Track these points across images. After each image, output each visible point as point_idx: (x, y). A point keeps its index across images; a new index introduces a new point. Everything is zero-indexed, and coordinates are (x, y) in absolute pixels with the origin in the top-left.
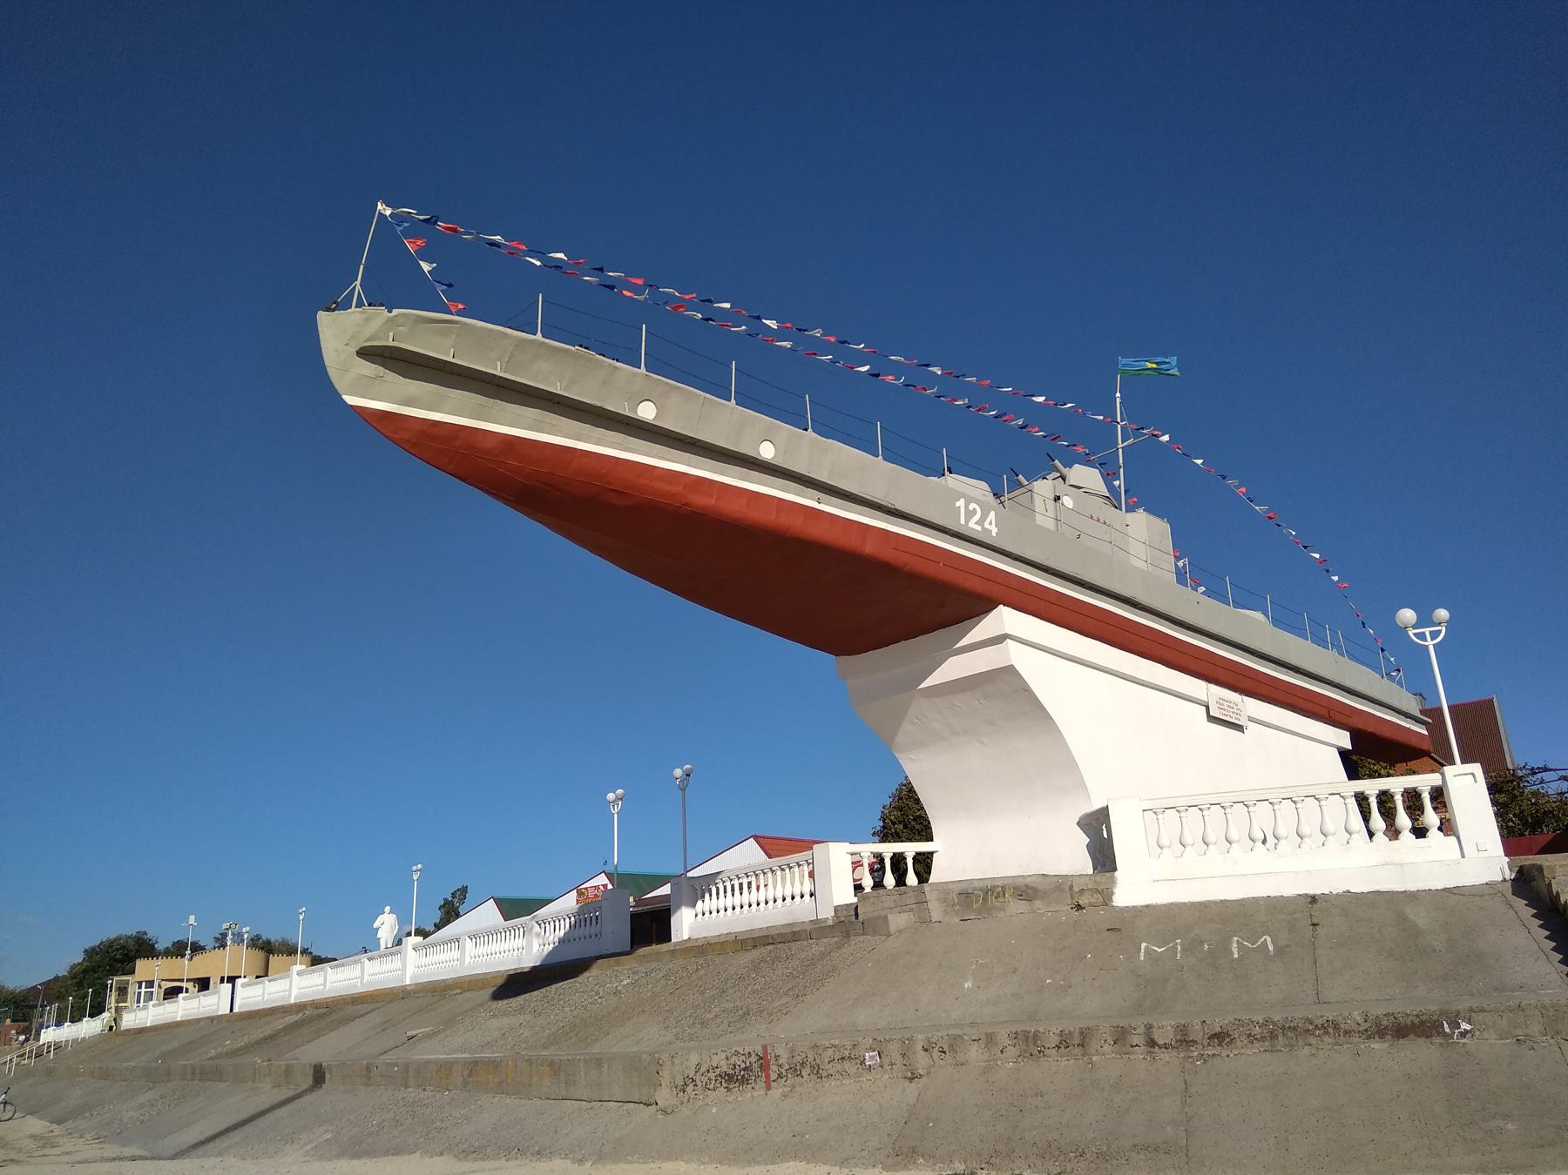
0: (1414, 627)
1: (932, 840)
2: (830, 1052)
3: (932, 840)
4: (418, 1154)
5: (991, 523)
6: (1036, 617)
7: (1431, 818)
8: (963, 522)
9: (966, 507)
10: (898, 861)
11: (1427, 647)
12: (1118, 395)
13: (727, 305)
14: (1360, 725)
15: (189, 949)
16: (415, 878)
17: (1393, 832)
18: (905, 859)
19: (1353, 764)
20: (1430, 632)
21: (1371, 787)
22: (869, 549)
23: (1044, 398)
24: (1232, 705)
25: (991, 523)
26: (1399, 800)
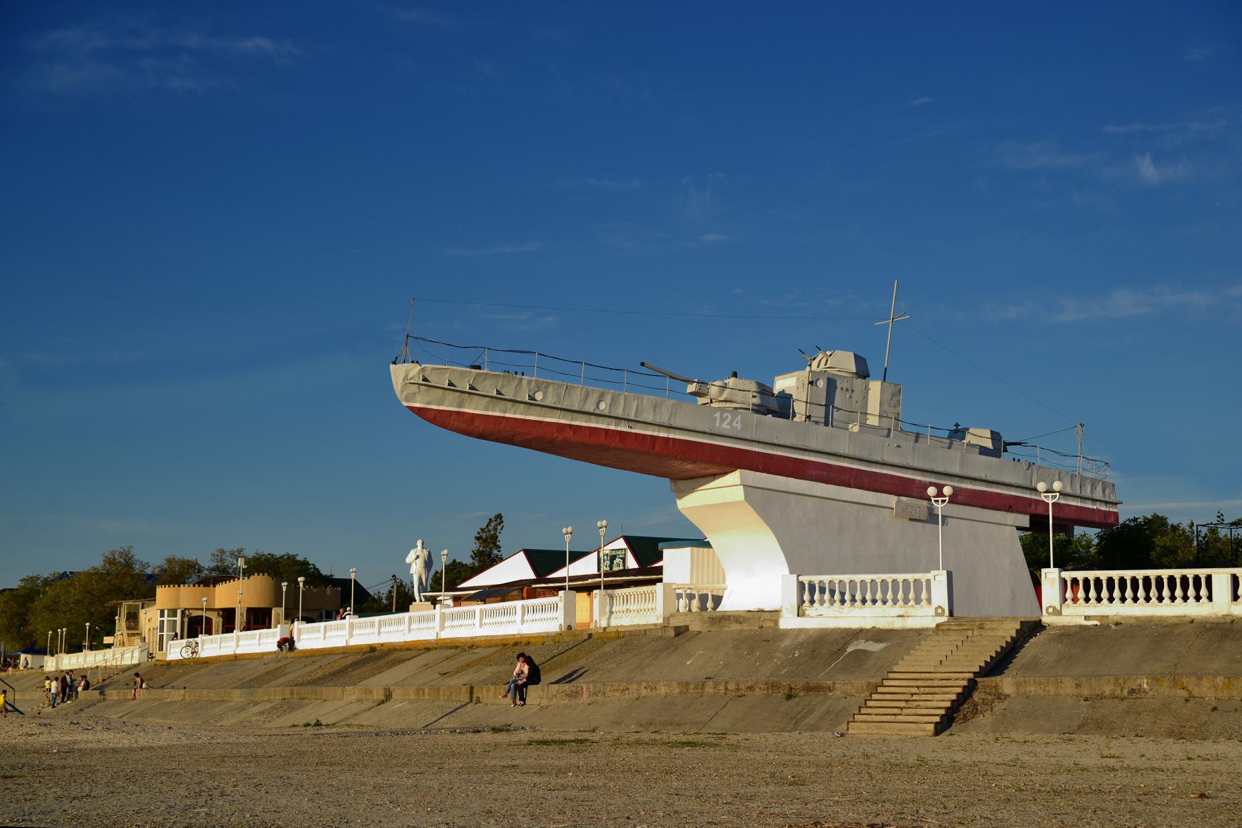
0: (934, 497)
1: (234, 609)
2: (609, 687)
3: (234, 609)
5: (737, 423)
7: (1204, 592)
8: (717, 425)
9: (721, 416)
11: (938, 507)
15: (88, 628)
16: (602, 534)
17: (832, 602)
18: (1188, 579)
20: (176, 620)
25: (737, 423)
26: (1117, 583)
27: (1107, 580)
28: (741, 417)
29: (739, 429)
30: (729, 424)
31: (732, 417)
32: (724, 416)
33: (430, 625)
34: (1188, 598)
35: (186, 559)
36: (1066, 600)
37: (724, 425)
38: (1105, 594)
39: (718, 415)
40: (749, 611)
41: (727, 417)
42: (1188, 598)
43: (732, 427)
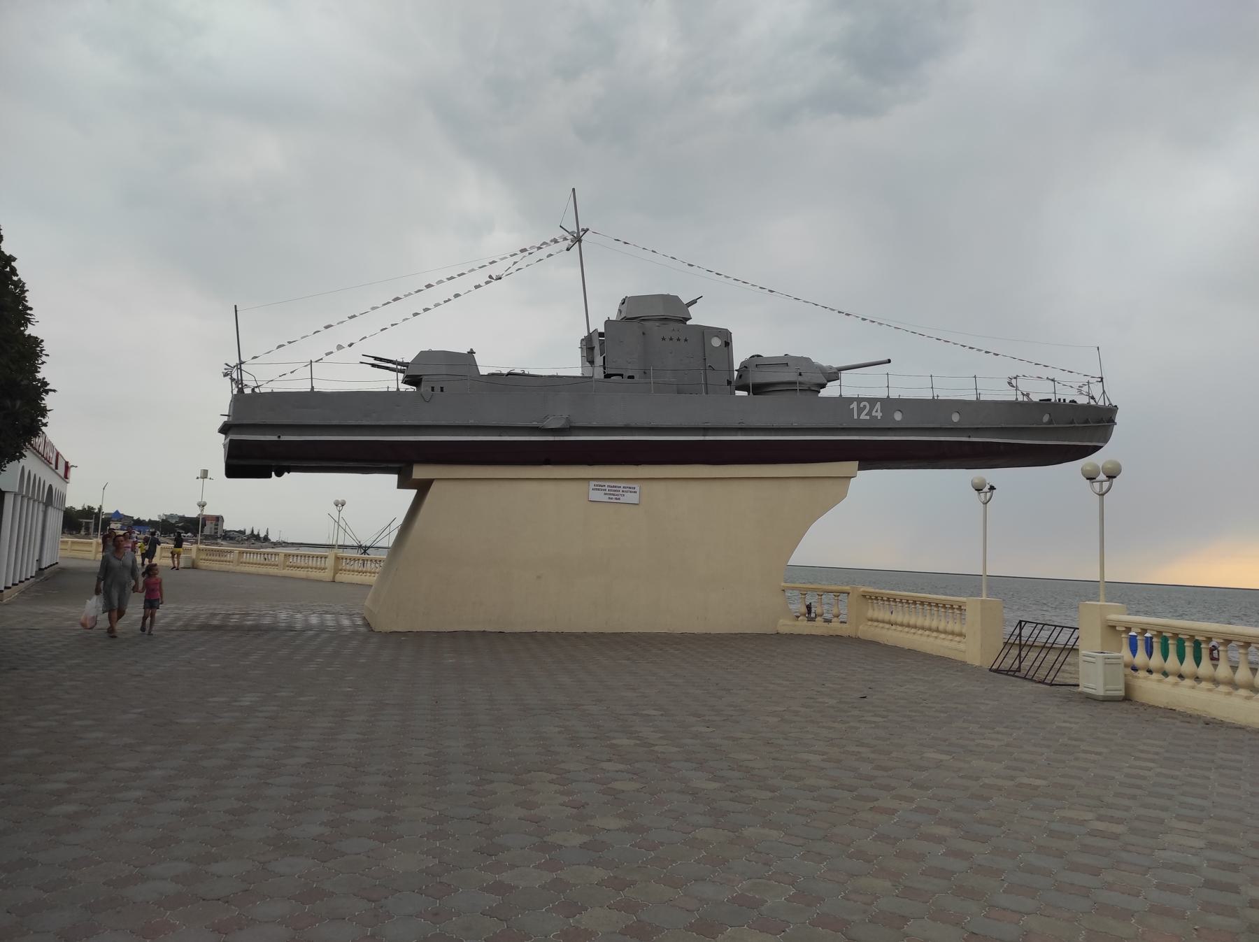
1: (399, 487)
3: (399, 487)
5: (877, 411)
8: (856, 417)
25: (877, 411)
29: (879, 418)
30: (869, 413)
32: (862, 406)
35: (48, 401)
39: (854, 405)
41: (865, 406)
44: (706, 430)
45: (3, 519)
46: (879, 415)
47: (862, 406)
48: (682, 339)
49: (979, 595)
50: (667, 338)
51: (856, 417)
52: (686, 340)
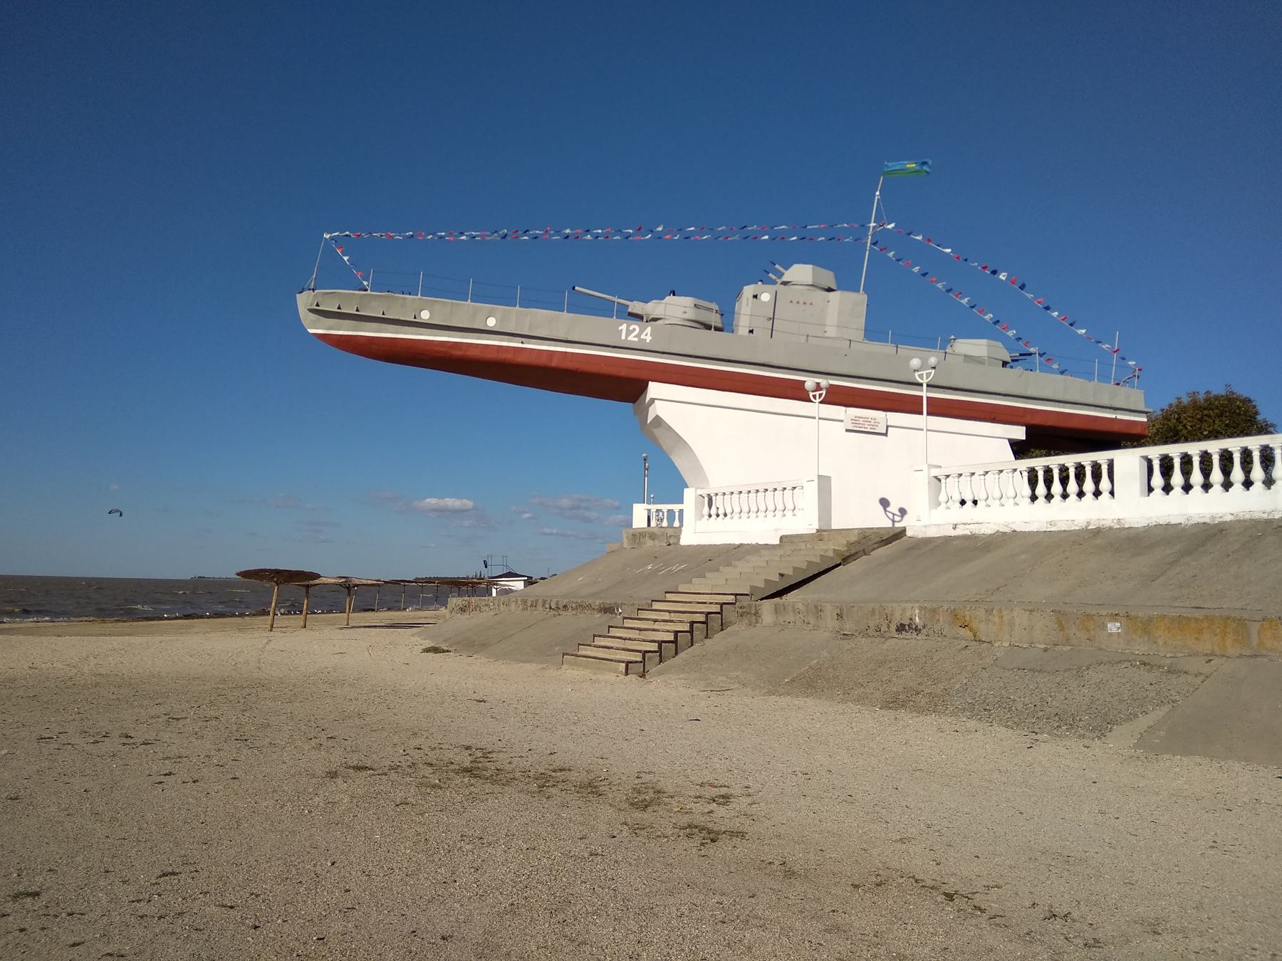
1: (683, 503)
3: (683, 503)
4: (1121, 739)
5: (646, 335)
6: (672, 383)
8: (623, 338)
10: (671, 512)
12: (878, 193)
13: (692, 229)
14: (1037, 421)
19: (1020, 449)
21: (1039, 463)
22: (554, 363)
23: (662, 226)
24: (869, 420)
25: (646, 335)
26: (1256, 456)
27: (1202, 457)
28: (652, 330)
29: (648, 341)
30: (638, 336)
31: (640, 330)
32: (631, 328)
33: (266, 617)
34: (1053, 497)
36: (1150, 489)
37: (631, 338)
38: (1197, 477)
40: (200, 577)
41: (634, 329)
42: (1053, 497)
43: (640, 339)
44: (913, 350)
45: (703, 544)
46: (649, 339)
47: (631, 328)
48: (808, 303)
49: (417, 295)
50: (795, 301)
51: (623, 338)
52: (811, 304)
